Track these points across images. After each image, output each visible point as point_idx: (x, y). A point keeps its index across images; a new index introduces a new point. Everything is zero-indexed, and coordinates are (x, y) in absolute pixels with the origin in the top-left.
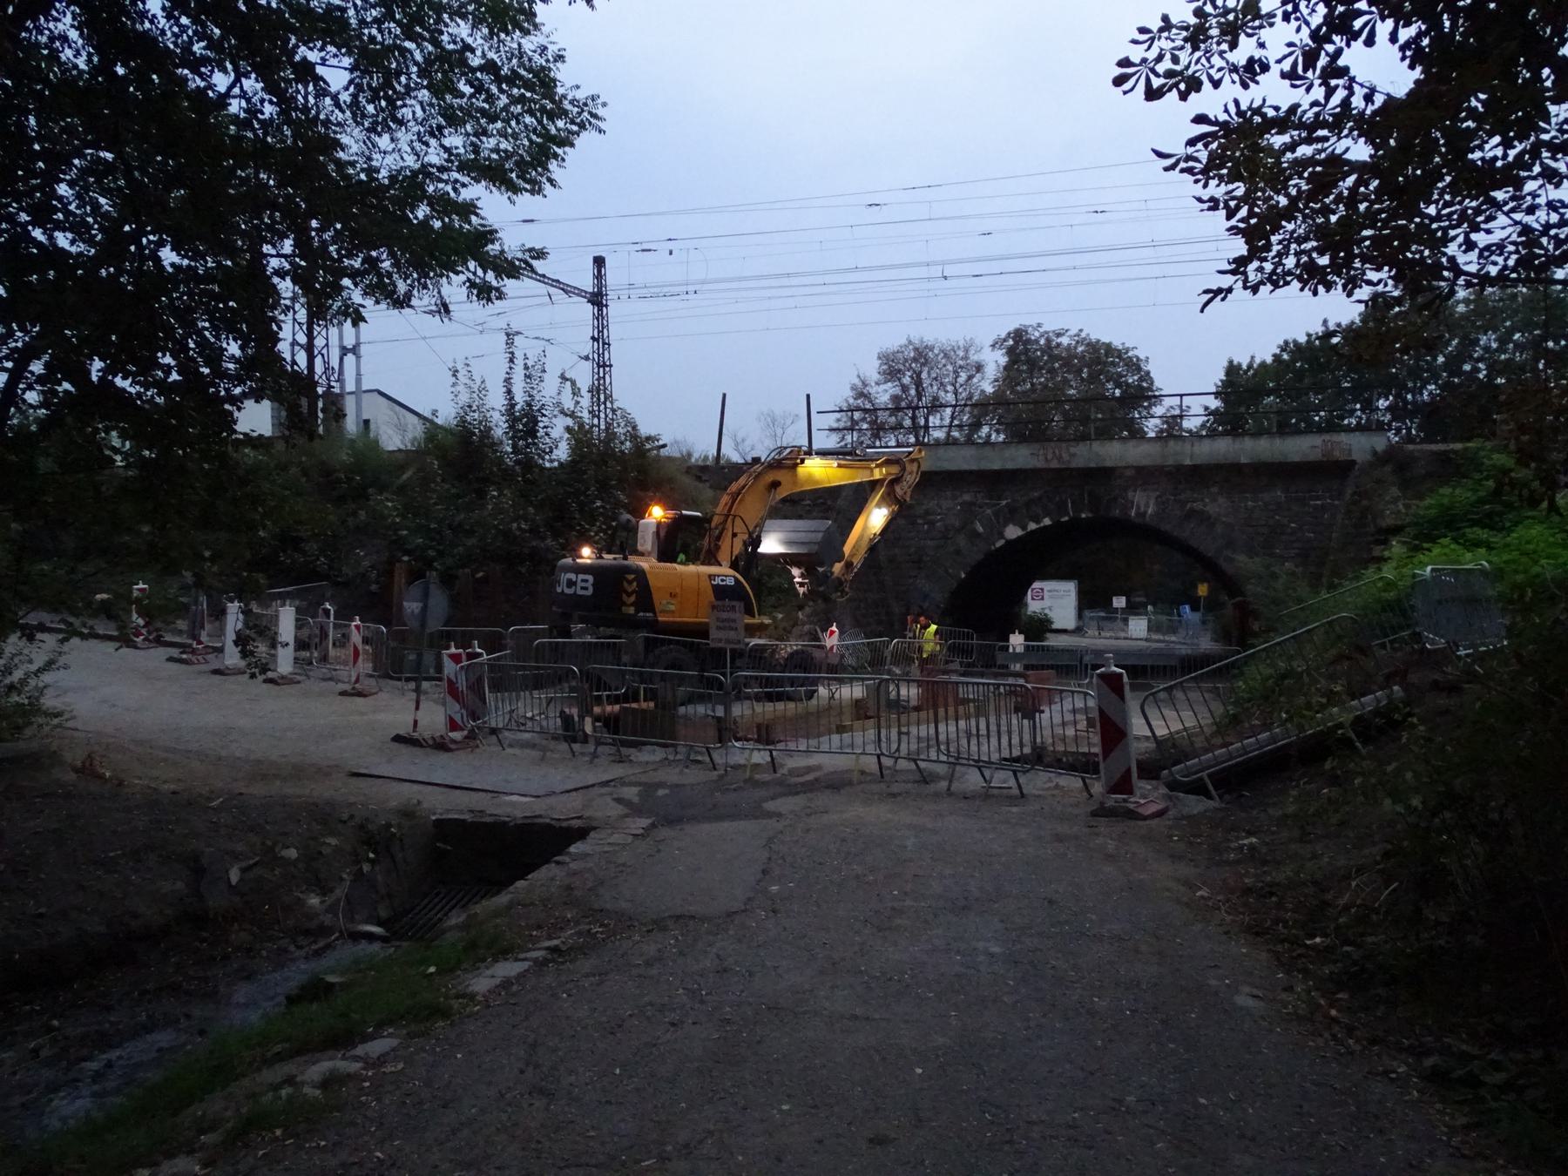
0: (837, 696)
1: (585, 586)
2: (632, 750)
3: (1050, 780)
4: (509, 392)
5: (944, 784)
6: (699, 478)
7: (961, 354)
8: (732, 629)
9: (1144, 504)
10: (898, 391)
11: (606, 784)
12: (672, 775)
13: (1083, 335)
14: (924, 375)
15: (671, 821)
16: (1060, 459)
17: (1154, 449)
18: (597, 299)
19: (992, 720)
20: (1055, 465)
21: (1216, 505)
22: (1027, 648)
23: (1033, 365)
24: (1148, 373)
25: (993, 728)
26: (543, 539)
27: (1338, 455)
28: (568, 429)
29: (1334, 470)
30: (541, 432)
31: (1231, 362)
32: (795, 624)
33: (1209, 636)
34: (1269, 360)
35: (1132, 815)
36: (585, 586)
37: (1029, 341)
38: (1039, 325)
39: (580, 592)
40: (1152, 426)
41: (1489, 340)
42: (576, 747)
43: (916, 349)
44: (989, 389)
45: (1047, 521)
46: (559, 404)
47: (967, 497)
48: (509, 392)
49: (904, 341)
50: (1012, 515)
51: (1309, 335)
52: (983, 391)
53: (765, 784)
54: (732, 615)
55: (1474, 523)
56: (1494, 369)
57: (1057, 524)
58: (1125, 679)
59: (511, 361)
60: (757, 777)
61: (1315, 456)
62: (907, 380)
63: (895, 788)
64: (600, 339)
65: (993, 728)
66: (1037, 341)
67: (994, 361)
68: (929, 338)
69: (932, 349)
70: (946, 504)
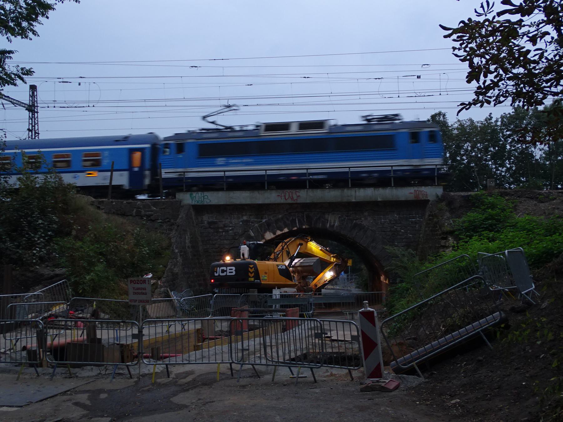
0: (186, 327)
1: (231, 271)
2: (77, 370)
3: (327, 371)
5: (268, 377)
6: (99, 208)
8: (143, 294)
11: (64, 393)
12: (105, 384)
16: (292, 198)
18: (32, 108)
19: (273, 336)
20: (290, 201)
21: (367, 221)
25: (274, 341)
26: (4, 242)
27: (421, 197)
29: (420, 204)
33: (354, 285)
35: (384, 390)
36: (231, 271)
39: (228, 274)
41: (467, 146)
42: (39, 369)
45: (286, 230)
47: (245, 218)
50: (269, 227)
53: (165, 385)
54: (143, 286)
55: (486, 229)
58: (375, 314)
61: (411, 197)
63: (243, 382)
65: (274, 341)
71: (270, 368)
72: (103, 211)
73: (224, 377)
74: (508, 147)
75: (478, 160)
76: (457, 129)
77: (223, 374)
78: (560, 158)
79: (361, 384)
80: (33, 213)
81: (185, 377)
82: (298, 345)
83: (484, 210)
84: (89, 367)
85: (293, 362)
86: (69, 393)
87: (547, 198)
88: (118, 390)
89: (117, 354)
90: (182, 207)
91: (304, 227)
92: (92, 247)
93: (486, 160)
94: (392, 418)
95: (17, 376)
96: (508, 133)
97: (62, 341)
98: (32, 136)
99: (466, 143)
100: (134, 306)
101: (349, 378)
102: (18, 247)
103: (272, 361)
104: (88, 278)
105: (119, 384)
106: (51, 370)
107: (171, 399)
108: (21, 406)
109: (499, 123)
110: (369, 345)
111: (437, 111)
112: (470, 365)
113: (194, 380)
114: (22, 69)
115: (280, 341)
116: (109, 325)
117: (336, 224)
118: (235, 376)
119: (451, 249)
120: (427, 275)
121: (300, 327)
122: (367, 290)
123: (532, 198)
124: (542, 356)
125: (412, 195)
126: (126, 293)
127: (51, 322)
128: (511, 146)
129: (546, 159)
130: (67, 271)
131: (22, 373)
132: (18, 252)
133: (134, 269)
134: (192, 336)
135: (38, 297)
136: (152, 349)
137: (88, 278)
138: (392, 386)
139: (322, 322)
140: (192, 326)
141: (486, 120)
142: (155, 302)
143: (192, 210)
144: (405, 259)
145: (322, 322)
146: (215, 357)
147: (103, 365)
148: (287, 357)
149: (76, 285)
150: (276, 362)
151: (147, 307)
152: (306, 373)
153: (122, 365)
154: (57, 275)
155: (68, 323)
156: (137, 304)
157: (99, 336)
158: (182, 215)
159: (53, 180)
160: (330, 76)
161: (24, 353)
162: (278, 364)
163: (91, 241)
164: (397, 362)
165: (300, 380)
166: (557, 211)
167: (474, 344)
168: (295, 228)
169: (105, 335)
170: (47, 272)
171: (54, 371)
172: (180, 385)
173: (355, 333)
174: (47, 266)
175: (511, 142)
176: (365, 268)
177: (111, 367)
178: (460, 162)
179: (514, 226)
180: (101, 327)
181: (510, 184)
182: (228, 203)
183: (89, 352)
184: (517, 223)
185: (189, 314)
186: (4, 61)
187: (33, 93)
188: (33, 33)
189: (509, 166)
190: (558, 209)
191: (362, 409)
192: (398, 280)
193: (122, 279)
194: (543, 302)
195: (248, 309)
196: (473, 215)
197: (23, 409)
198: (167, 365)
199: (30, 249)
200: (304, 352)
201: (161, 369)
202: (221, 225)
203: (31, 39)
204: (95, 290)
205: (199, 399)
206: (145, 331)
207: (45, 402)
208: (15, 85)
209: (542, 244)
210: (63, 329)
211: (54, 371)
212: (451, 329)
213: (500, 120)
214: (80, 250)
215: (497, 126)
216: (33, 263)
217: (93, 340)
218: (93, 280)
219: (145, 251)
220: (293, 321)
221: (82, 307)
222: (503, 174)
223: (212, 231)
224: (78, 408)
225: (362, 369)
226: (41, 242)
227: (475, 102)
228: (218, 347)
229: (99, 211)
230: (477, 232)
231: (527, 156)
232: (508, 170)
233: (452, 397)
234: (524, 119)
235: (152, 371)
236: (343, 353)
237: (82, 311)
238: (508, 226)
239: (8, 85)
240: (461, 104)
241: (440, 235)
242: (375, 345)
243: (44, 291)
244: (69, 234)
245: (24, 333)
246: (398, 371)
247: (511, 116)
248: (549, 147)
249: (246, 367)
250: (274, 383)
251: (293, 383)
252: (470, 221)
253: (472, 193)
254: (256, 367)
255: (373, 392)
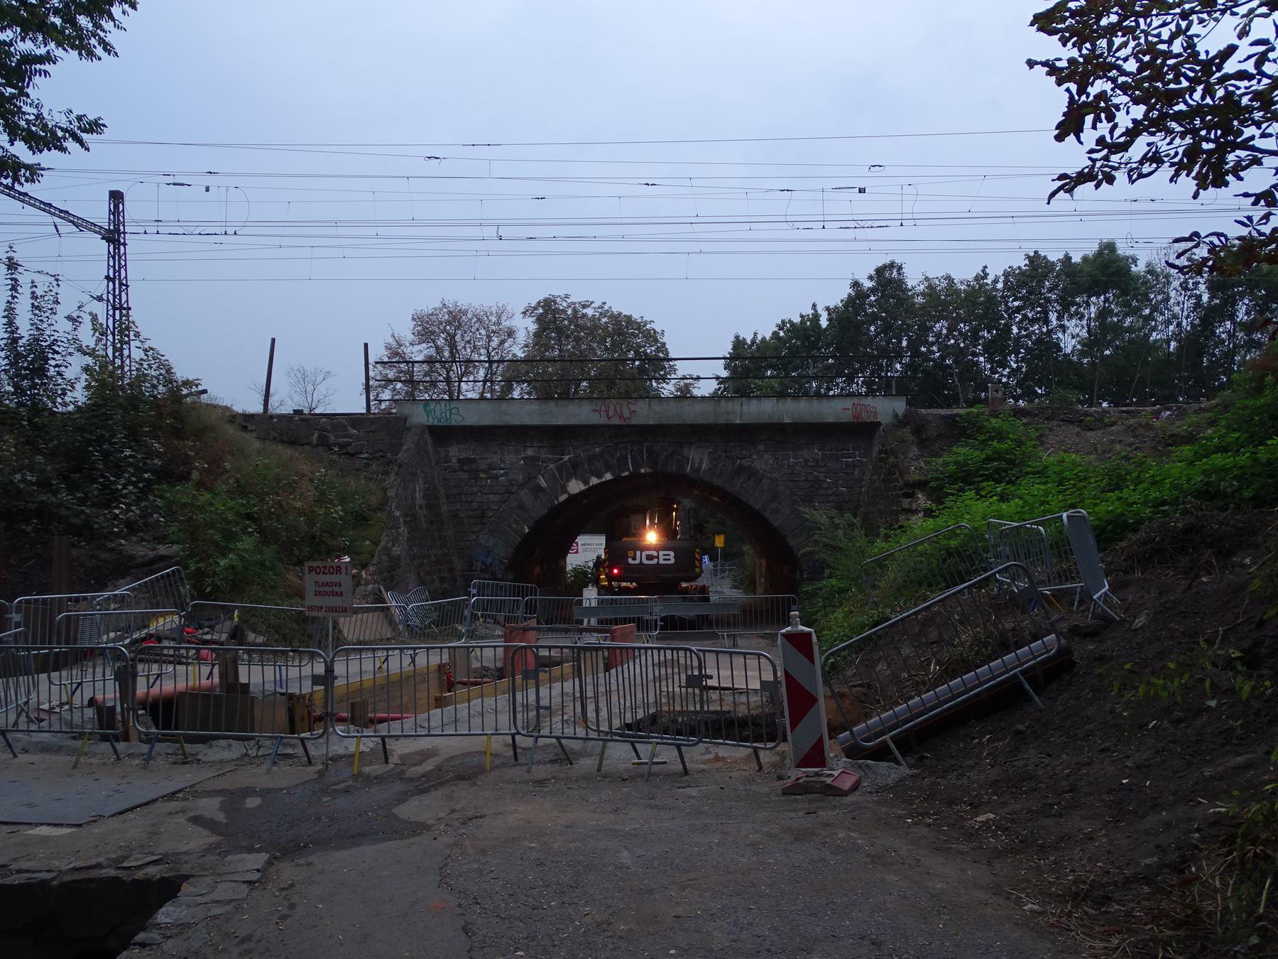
0: (407, 660)
3: (707, 751)
4: (10, 323)
5: (587, 764)
6: (244, 428)
7: (494, 319)
9: (699, 459)
10: (432, 351)
11: (172, 796)
13: (606, 307)
14: (458, 338)
15: (287, 850)
16: (621, 416)
17: (709, 407)
18: (114, 236)
19: (589, 679)
20: (616, 421)
21: (762, 460)
22: (600, 602)
23: (560, 331)
24: (664, 344)
25: (590, 688)
26: (55, 492)
27: (865, 417)
28: (87, 369)
29: (862, 430)
30: (52, 372)
31: (737, 337)
32: (358, 584)
34: (768, 336)
35: (831, 791)
37: (557, 311)
38: (567, 296)
39: (661, 562)
40: (668, 389)
41: (941, 326)
42: (121, 746)
43: (450, 313)
44: (521, 355)
45: (608, 476)
46: (75, 340)
47: (530, 452)
48: (10, 323)
49: (438, 305)
50: (575, 470)
51: (802, 316)
52: (514, 355)
53: (380, 779)
54: (335, 578)
55: (988, 478)
56: (944, 349)
57: (617, 480)
58: (814, 639)
59: (14, 288)
60: (367, 769)
61: (847, 417)
62: (441, 342)
63: (540, 772)
64: (117, 278)
65: (590, 688)
66: (564, 311)
67: (525, 327)
68: (463, 303)
69: (465, 313)
70: (510, 458)
71: (591, 743)
72: (254, 434)
73: (498, 762)
74: (1015, 330)
75: (959, 353)
76: (923, 294)
77: (497, 755)
78: (1107, 352)
79: (780, 778)
80: (114, 436)
81: (420, 763)
82: (639, 696)
83: (984, 441)
84: (223, 742)
85: (634, 730)
86: (181, 795)
87: (1100, 422)
88: (282, 789)
89: (282, 715)
90: (409, 429)
91: (643, 471)
92: (231, 504)
93: (975, 354)
94: (868, 855)
95: (74, 758)
96: (1016, 304)
97: (168, 687)
98: (114, 289)
99: (938, 321)
100: (314, 618)
101: (754, 765)
102: (83, 502)
103: (599, 731)
104: (222, 563)
105: (286, 776)
106: (145, 748)
107: (395, 810)
108: (80, 825)
109: (1000, 286)
110: (801, 700)
111: (887, 261)
112: (999, 740)
113: (439, 768)
114: (79, 118)
115: (602, 689)
116: (262, 655)
117: (704, 466)
118: (522, 760)
119: (921, 514)
120: (880, 564)
121: (637, 661)
122: (754, 591)
123: (1071, 422)
124: (1151, 725)
125: (849, 412)
126: (300, 594)
127: (149, 650)
128: (1019, 329)
129: (1083, 354)
130: (182, 550)
131: (86, 754)
132: (82, 512)
133: (311, 546)
134: (433, 676)
135: (122, 600)
136: (353, 705)
137: (222, 563)
138: (847, 784)
139: (701, 654)
140: (429, 658)
141: (977, 278)
142: (356, 611)
143: (427, 436)
144: (840, 532)
145: (701, 654)
146: (481, 721)
147: (253, 738)
148: (616, 723)
149: (199, 576)
150: (607, 733)
151: (342, 620)
152: (668, 755)
153: (293, 739)
154: (162, 558)
155: (183, 651)
156: (321, 614)
157: (243, 679)
158: (409, 444)
159: (154, 373)
160: (694, 182)
161: (89, 713)
162: (608, 737)
163: (228, 491)
164: (852, 732)
165: (655, 769)
166: (1118, 447)
167: (1002, 700)
168: (626, 473)
169: (255, 675)
170: (140, 550)
171: (151, 750)
172: (411, 780)
173: (768, 676)
174: (143, 540)
175: (1021, 321)
176: (751, 551)
177: (268, 743)
178: (926, 357)
179: (1042, 473)
180: (249, 661)
181: (1016, 399)
182: (497, 423)
183: (225, 711)
184: (1046, 467)
185: (419, 634)
186: (30, 79)
187: (116, 206)
188: (105, 49)
189: (1015, 366)
190: (1120, 441)
191: (800, 836)
192: (827, 572)
193: (291, 567)
194: (1135, 617)
195: (535, 625)
196: (963, 452)
197: (83, 830)
198: (383, 738)
199: (108, 506)
200: (652, 711)
201: (371, 745)
202: (483, 465)
203: (100, 59)
204: (238, 585)
205: (453, 811)
206: (339, 669)
207: (131, 815)
208: (64, 150)
209: (1109, 506)
210: (171, 662)
211: (151, 750)
212: (950, 671)
213: (1002, 278)
214: (208, 508)
215: (995, 289)
216: (113, 532)
217: (233, 688)
218: (233, 567)
219: (336, 512)
220: (649, 652)
221: (210, 619)
222: (1004, 380)
223: (465, 476)
224: (199, 828)
225: (783, 747)
226: (131, 492)
227: (1082, 177)
228: (490, 701)
229: (245, 435)
230: (973, 483)
231: (1047, 346)
232: (1014, 372)
233: (976, 807)
234: (1045, 277)
235: (352, 749)
236: (728, 712)
237: (211, 627)
238: (1028, 473)
239: (49, 150)
240: (1060, 178)
241: (901, 489)
242: (813, 700)
243: (133, 589)
244: (185, 478)
245: (99, 670)
246: (853, 752)
247: (1022, 273)
248: (1089, 332)
249: (541, 741)
250: (601, 775)
251: (641, 776)
252: (956, 463)
253: (962, 411)
254: (563, 741)
255: (809, 796)
